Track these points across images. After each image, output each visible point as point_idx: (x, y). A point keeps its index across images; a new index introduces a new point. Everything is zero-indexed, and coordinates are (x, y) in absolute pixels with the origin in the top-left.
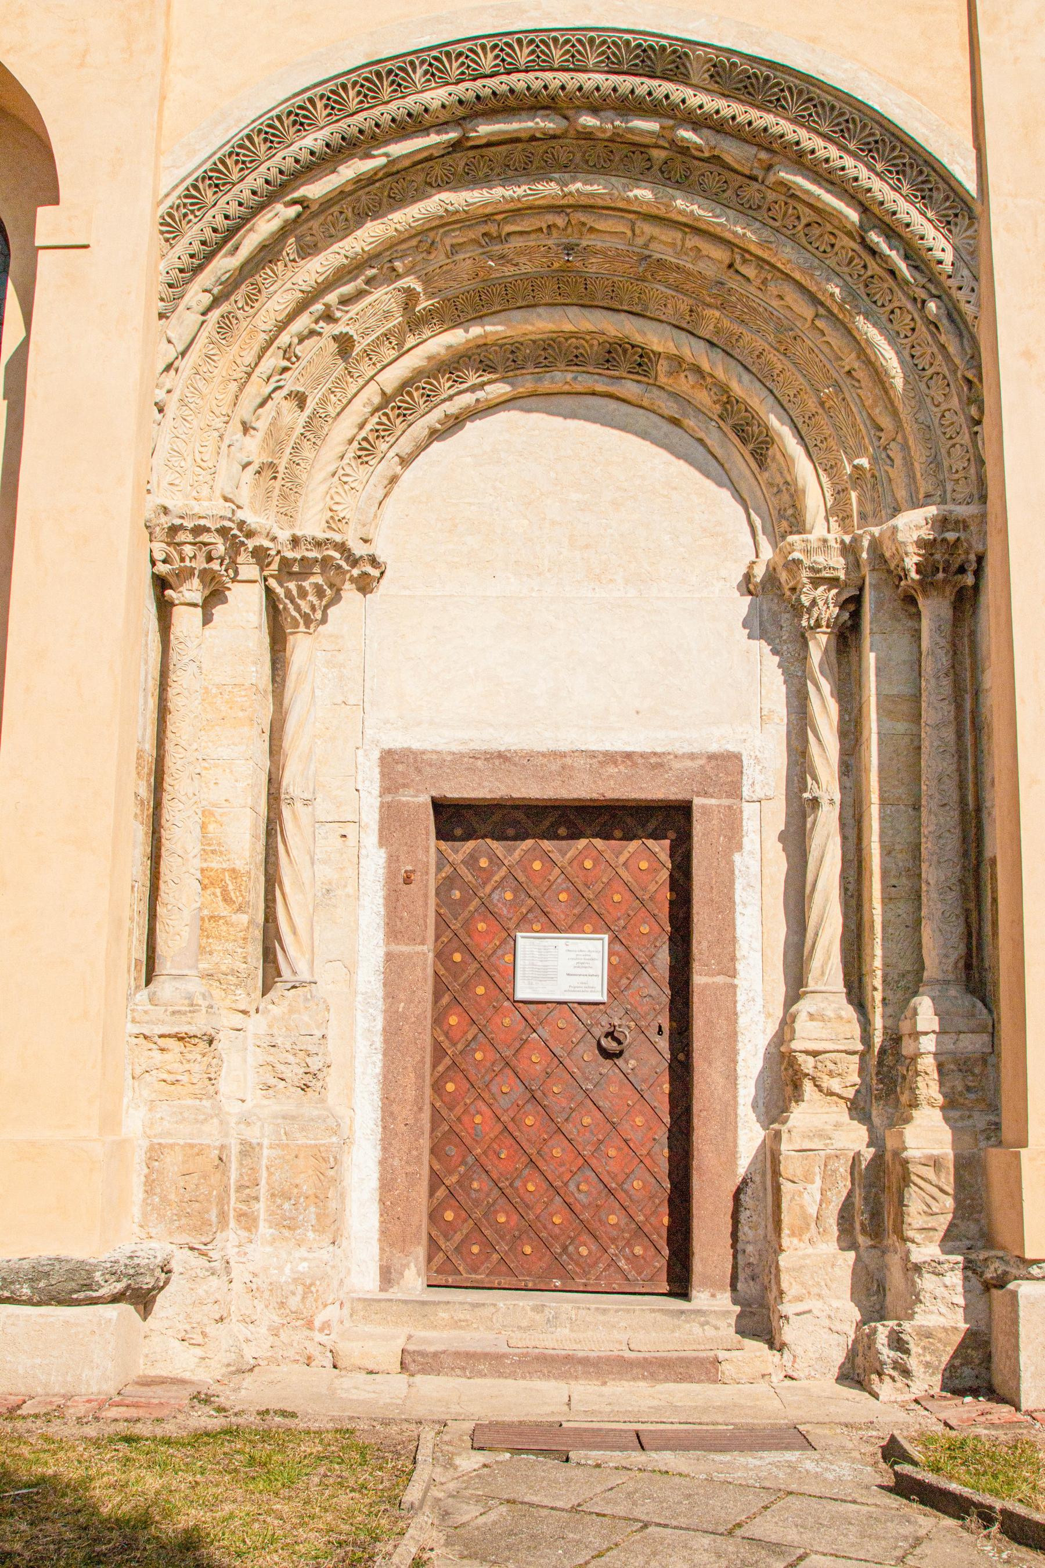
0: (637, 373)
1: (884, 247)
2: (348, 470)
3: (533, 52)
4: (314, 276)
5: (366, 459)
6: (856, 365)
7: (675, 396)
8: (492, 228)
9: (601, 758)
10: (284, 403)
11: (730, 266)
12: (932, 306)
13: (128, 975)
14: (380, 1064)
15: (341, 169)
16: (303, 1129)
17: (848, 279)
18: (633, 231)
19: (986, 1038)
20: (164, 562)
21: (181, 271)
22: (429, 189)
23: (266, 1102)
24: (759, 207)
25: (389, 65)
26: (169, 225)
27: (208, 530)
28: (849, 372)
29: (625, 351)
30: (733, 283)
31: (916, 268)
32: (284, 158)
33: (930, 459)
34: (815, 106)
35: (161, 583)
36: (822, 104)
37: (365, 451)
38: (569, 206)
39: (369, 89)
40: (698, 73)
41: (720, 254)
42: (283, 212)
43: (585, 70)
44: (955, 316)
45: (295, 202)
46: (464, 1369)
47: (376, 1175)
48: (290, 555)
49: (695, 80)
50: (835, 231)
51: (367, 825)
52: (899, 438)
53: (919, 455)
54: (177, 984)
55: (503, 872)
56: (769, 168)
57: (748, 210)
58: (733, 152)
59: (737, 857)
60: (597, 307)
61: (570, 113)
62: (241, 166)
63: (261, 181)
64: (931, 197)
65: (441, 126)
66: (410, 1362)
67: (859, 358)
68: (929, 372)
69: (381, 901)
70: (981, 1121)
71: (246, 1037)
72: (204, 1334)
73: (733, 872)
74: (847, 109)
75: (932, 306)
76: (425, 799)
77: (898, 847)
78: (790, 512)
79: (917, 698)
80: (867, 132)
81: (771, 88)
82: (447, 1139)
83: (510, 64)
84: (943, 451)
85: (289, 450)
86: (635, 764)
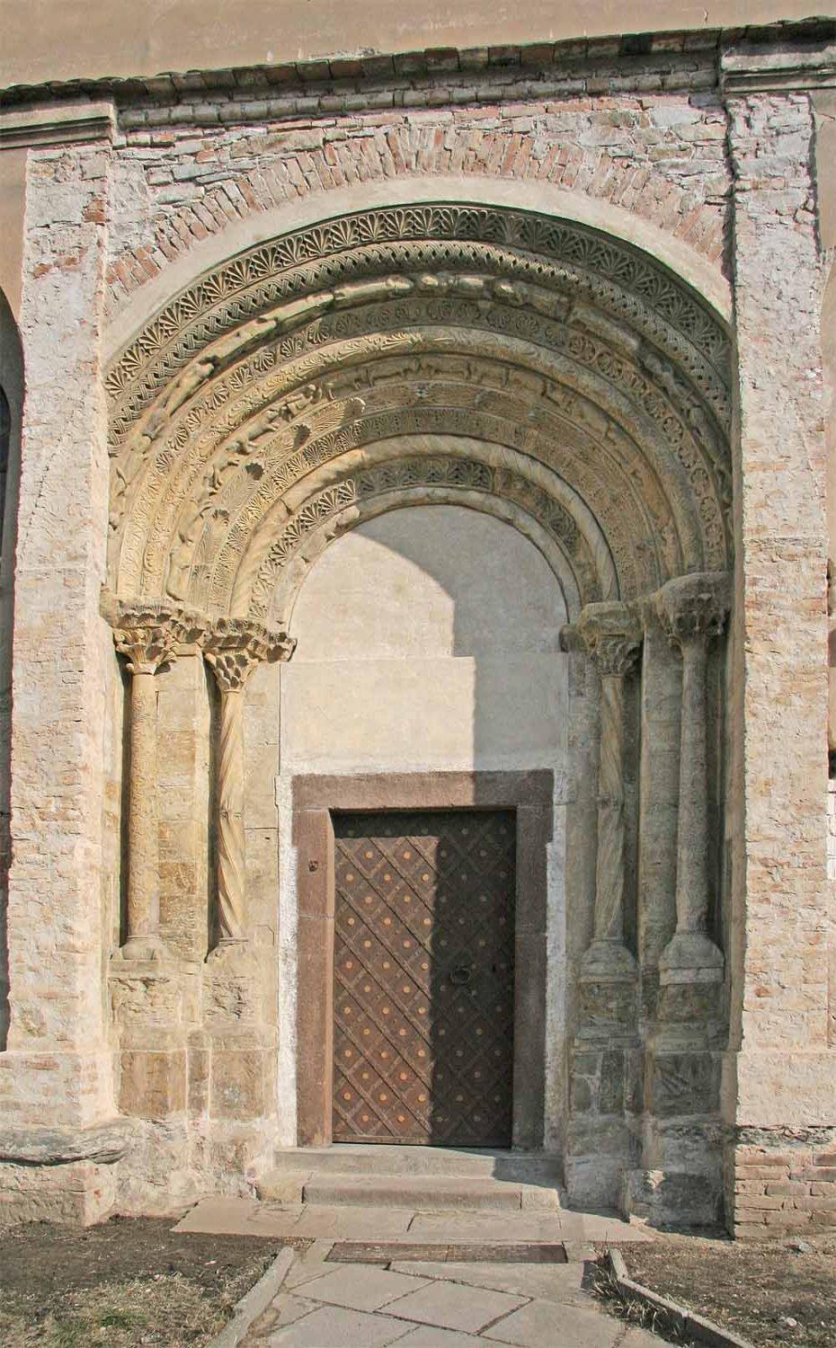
8: (362, 373)
13: (113, 937)
14: (295, 996)
18: (469, 369)
19: (719, 972)
20: (124, 643)
21: (125, 420)
25: (273, 244)
26: (112, 384)
27: (152, 617)
29: (469, 468)
31: (682, 384)
35: (123, 658)
41: (538, 384)
43: (424, 238)
45: (207, 361)
47: (294, 1071)
49: (509, 239)
50: (622, 359)
51: (284, 830)
52: (671, 522)
53: (686, 536)
56: (570, 309)
57: (556, 346)
58: (544, 298)
59: (549, 846)
62: (165, 334)
65: (315, 291)
67: (641, 461)
68: (693, 469)
69: (294, 883)
70: (711, 1031)
72: (164, 1178)
73: (545, 856)
75: (694, 412)
81: (570, 240)
83: (365, 237)
84: (703, 532)
85: (217, 556)
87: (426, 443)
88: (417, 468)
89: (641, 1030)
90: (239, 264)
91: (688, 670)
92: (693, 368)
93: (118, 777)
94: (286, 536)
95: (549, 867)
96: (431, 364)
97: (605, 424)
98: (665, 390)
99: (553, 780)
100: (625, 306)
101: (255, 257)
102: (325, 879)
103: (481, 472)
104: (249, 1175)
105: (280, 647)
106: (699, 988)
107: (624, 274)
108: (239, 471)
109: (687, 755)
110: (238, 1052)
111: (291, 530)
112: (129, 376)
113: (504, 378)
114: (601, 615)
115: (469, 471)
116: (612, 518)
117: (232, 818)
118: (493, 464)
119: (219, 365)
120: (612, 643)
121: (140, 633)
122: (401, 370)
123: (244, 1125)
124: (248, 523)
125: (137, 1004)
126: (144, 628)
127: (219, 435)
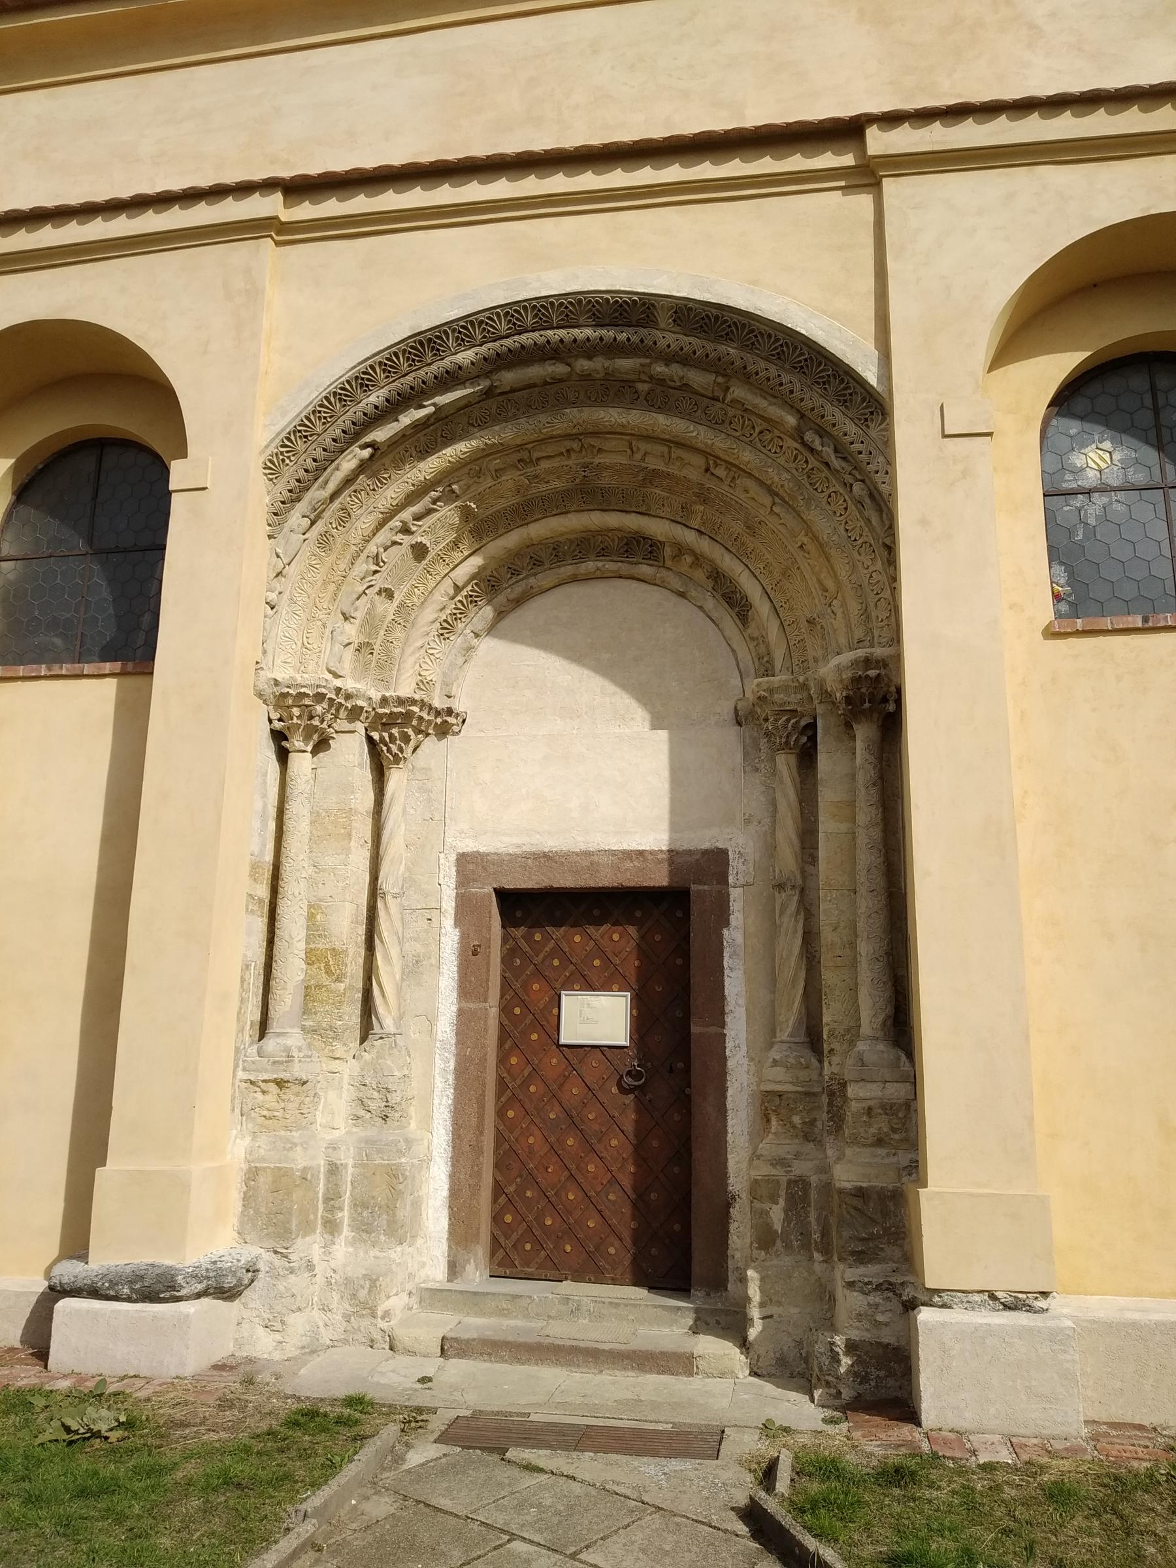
1: (817, 445)
2: (433, 645)
3: (536, 315)
6: (805, 540)
7: (680, 574)
8: (525, 455)
9: (620, 856)
10: (377, 597)
11: (707, 470)
12: (857, 487)
13: (250, 1032)
15: (401, 417)
16: (379, 1151)
20: (280, 720)
21: (283, 503)
22: (471, 428)
23: (355, 1130)
25: (429, 335)
27: (308, 695)
28: (801, 546)
30: (711, 484)
31: (844, 459)
35: (279, 737)
37: (446, 629)
38: (581, 434)
39: (416, 355)
40: (664, 320)
41: (699, 461)
44: (875, 493)
46: (490, 1354)
47: (447, 1187)
48: (380, 711)
49: (662, 325)
53: (854, 607)
54: (279, 1040)
55: (552, 944)
56: (728, 389)
57: (716, 424)
58: (699, 379)
59: (725, 932)
61: (569, 360)
63: (338, 431)
64: (851, 400)
65: (473, 379)
66: (448, 1348)
71: (342, 1078)
72: (283, 1323)
75: (857, 487)
76: (489, 890)
77: (842, 924)
78: (766, 659)
79: (852, 804)
81: (722, 324)
82: (507, 1157)
84: (872, 605)
85: (382, 632)
86: (646, 860)
87: (595, 520)
88: (586, 546)
89: (830, 1152)
90: (396, 354)
91: (859, 744)
93: (269, 857)
95: (726, 955)
97: (770, 499)
98: (827, 464)
99: (728, 860)
100: (781, 384)
101: (412, 347)
102: (488, 964)
104: (383, 1318)
106: (889, 1108)
108: (405, 550)
109: (862, 839)
110: (382, 1165)
111: (460, 606)
112: (287, 461)
113: (667, 456)
114: (771, 691)
115: (637, 549)
117: (389, 898)
121: (296, 711)
123: (381, 1255)
124: (415, 600)
125: (268, 1110)
126: (299, 706)
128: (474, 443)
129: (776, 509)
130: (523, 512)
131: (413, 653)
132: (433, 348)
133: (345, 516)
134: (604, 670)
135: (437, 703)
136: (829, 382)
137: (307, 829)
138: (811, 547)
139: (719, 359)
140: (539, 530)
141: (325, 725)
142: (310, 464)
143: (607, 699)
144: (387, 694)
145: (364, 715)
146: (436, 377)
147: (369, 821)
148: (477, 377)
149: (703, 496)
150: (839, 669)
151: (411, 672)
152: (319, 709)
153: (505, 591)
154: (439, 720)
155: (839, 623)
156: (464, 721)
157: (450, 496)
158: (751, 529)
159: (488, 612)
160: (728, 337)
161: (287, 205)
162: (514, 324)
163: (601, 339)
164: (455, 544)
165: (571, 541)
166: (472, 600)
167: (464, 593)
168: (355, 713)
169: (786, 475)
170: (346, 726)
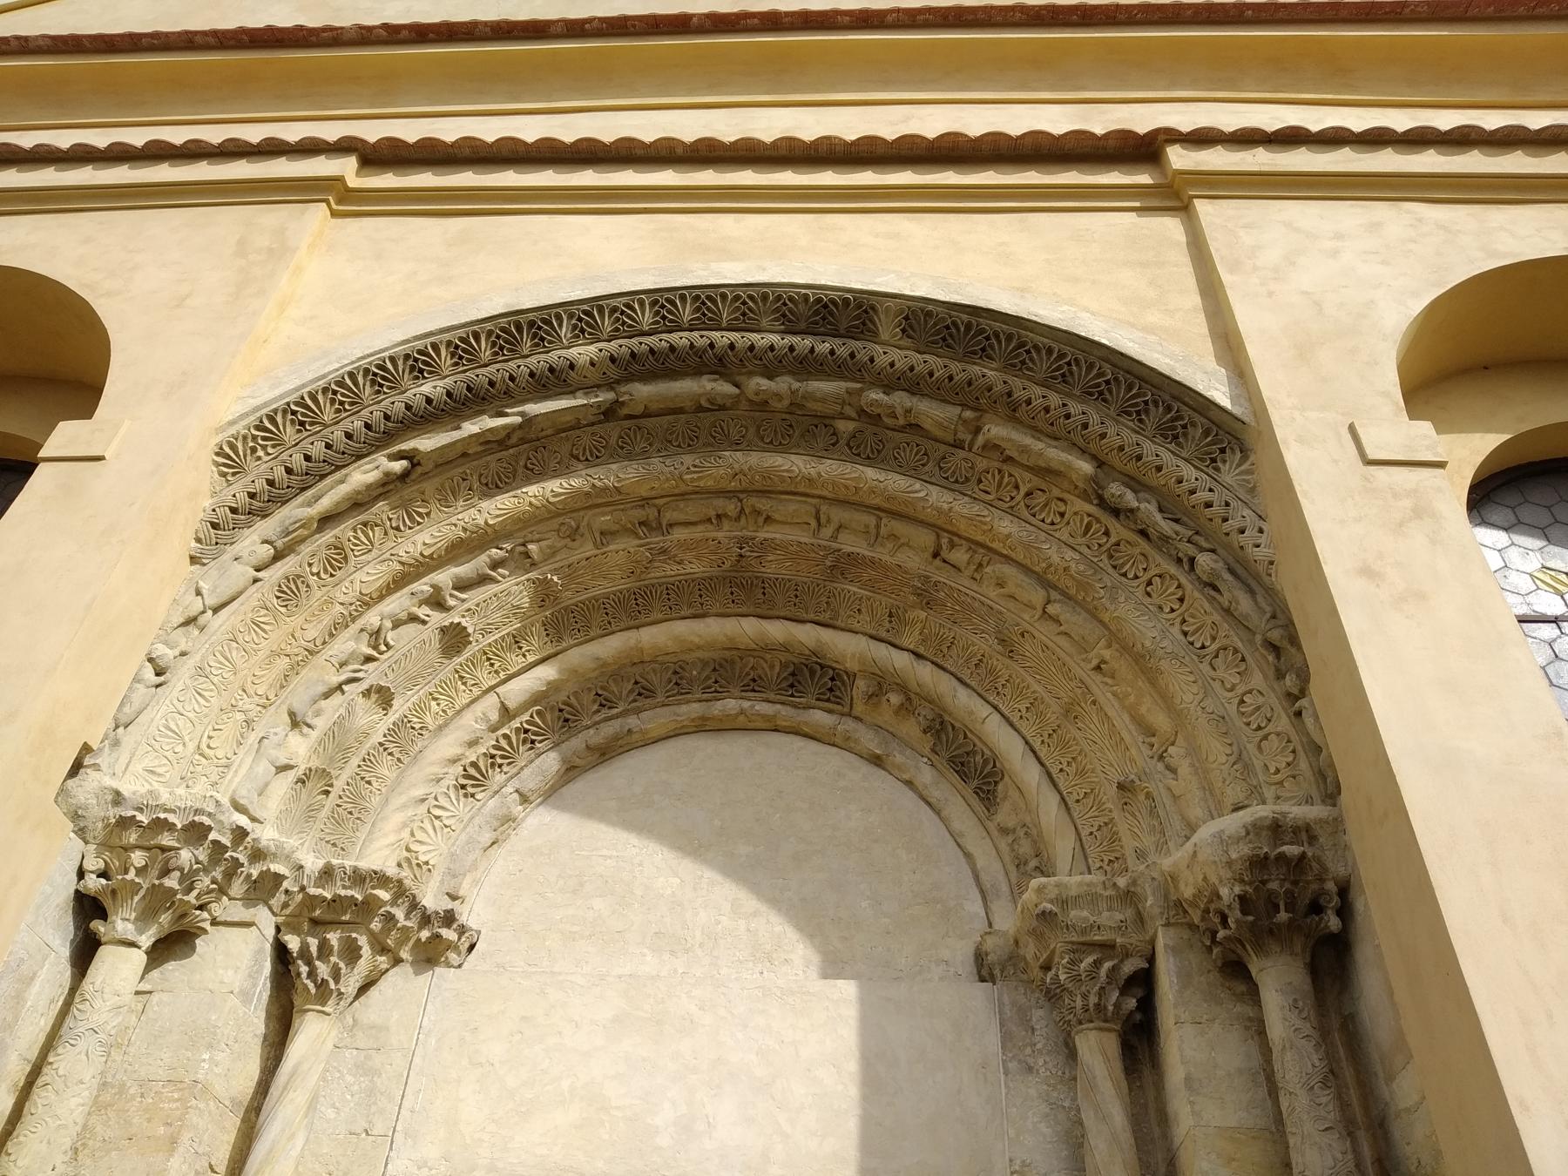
0: (828, 700)
1: (1130, 499)
2: (443, 801)
4: (420, 547)
5: (471, 790)
8: (652, 513)
10: (361, 700)
11: (936, 555)
17: (1086, 551)
20: (103, 874)
21: (234, 511)
22: (574, 462)
24: (967, 480)
25: (531, 316)
28: (1098, 668)
30: (940, 575)
31: (1177, 521)
32: (394, 403)
33: (1232, 759)
34: (1028, 352)
35: (89, 908)
36: (1035, 347)
37: (472, 780)
41: (925, 538)
42: (382, 464)
44: (1240, 570)
48: (312, 891)
49: (884, 336)
53: (1217, 751)
56: (978, 430)
57: (956, 483)
58: (933, 413)
60: (778, 618)
63: (358, 424)
65: (588, 389)
74: (1066, 349)
75: (1204, 560)
80: (1095, 372)
81: (974, 336)
83: (671, 321)
84: (1251, 748)
85: (355, 761)
87: (748, 629)
88: (729, 672)
90: (477, 336)
92: (1193, 492)
94: (493, 752)
96: (759, 506)
100: (1068, 416)
103: (832, 679)
105: (438, 936)
107: (1063, 375)
108: (428, 634)
111: (504, 743)
112: (260, 453)
113: (873, 531)
114: (1064, 902)
115: (812, 681)
116: (1064, 745)
118: (852, 666)
119: (419, 464)
120: (1090, 959)
121: (138, 858)
122: (712, 513)
124: (428, 719)
126: (148, 849)
127: (399, 567)
128: (576, 482)
129: (1051, 609)
130: (634, 606)
131: (404, 806)
132: (535, 336)
133: (338, 558)
134: (741, 871)
135: (431, 900)
136: (1147, 412)
137: (79, 1115)
138: (1122, 666)
139: (970, 384)
140: (661, 636)
141: (191, 898)
142: (297, 461)
143: (742, 923)
144: (335, 862)
145: (280, 897)
146: (532, 375)
147: (233, 1123)
148: (598, 386)
149: (927, 596)
150: (1221, 840)
151: (392, 838)
152: (185, 856)
153: (587, 732)
154: (425, 934)
155: (1187, 780)
156: (472, 947)
157: (524, 561)
158: (1008, 647)
159: (551, 762)
160: (985, 353)
161: (358, 174)
162: (664, 318)
163: (792, 349)
164: (516, 640)
165: (705, 663)
166: (528, 737)
167: (516, 724)
168: (264, 888)
169: (1069, 554)
170: (237, 911)
